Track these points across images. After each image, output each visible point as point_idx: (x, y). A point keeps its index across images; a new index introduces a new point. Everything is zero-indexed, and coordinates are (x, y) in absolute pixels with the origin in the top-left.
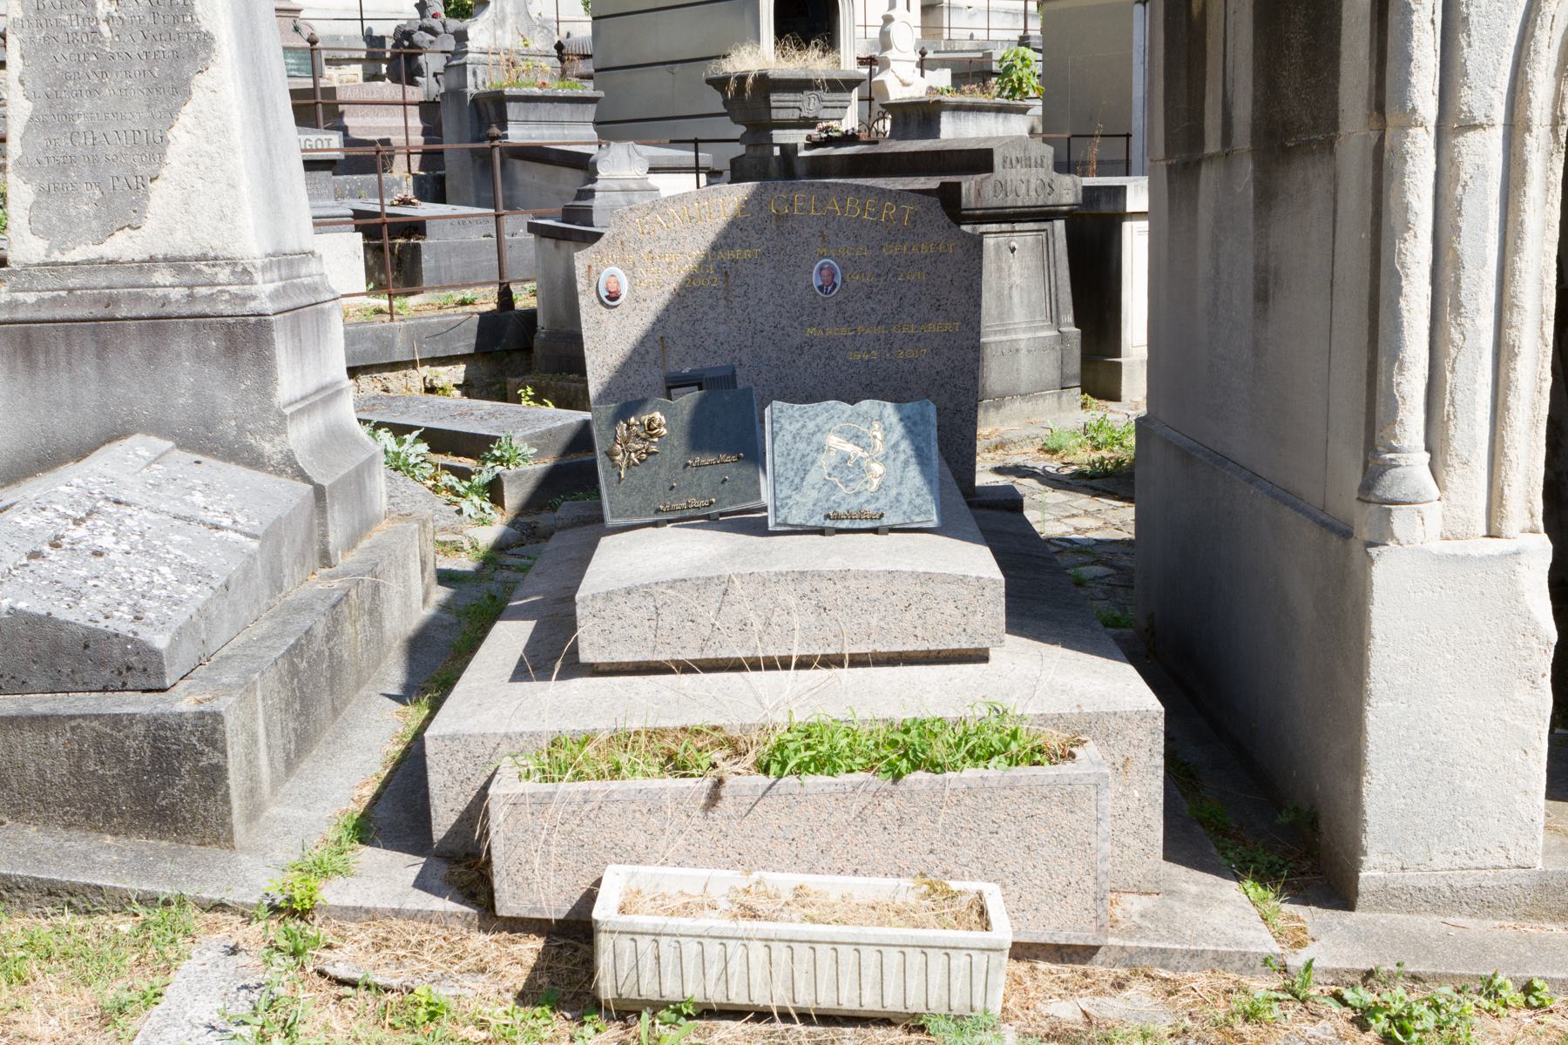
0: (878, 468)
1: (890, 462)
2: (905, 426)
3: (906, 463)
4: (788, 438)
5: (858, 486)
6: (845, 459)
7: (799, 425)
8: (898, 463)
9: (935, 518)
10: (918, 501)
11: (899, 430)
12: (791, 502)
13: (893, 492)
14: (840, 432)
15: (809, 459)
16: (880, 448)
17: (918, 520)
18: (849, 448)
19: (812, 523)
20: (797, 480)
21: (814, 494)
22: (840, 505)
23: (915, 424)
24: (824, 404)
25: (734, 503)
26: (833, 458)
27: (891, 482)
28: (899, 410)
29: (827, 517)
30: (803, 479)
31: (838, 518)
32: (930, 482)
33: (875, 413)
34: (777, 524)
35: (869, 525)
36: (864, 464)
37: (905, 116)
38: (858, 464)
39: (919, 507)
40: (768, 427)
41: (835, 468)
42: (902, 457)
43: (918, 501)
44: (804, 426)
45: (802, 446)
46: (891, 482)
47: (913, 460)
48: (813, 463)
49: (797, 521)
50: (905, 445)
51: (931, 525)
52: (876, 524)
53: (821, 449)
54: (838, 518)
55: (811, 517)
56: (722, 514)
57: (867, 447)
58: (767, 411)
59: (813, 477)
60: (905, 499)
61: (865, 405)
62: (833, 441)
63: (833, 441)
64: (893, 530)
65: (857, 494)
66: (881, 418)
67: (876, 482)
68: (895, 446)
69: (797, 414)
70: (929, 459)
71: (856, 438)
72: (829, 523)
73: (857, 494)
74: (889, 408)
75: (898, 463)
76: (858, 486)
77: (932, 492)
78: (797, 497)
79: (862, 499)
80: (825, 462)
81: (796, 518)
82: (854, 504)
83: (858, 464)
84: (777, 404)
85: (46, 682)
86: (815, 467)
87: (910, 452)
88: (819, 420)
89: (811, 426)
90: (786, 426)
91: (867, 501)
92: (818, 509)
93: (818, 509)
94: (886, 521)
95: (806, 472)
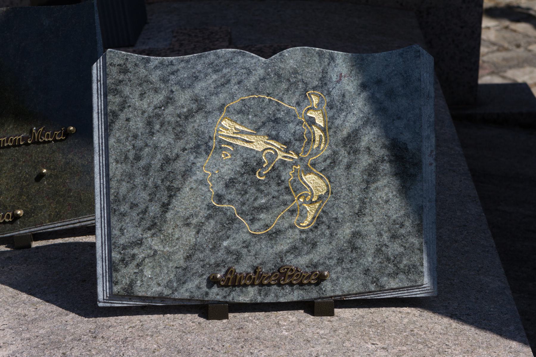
0: (314, 182)
1: (339, 171)
2: (372, 99)
3: (372, 173)
4: (138, 124)
5: (275, 219)
6: (251, 165)
7: (159, 98)
8: (357, 173)
9: (426, 280)
10: (395, 248)
11: (359, 107)
12: (140, 253)
13: (346, 231)
14: (242, 112)
15: (179, 165)
16: (320, 146)
17: (393, 285)
18: (259, 144)
19: (183, 293)
20: (154, 209)
21: (189, 236)
22: (238, 257)
23: (391, 94)
24: (211, 56)
25: (58, 217)
26: (226, 165)
27: (342, 211)
28: (359, 66)
29: (212, 282)
30: (165, 207)
31: (234, 281)
32: (419, 211)
33: (311, 74)
34: (113, 296)
35: (296, 295)
36: (288, 175)
37: (92, 247)
38: (276, 174)
39: (395, 260)
40: (97, 102)
41: (230, 184)
42: (365, 161)
43: (395, 248)
44: (169, 100)
45: (164, 140)
46: (342, 211)
47: (386, 167)
48: (186, 174)
49: (155, 290)
50: (370, 137)
51: (417, 293)
52: (312, 294)
53: (204, 145)
54: (234, 281)
55: (182, 282)
56: (37, 237)
57: (296, 142)
58: (96, 70)
59: (189, 201)
60: (369, 245)
61: (292, 57)
62: (227, 127)
63: (227, 127)
64: (344, 302)
65: (274, 235)
66: (323, 84)
67: (311, 211)
68: (351, 140)
69: (154, 77)
70: (418, 164)
71: (272, 124)
72: (216, 294)
73: (274, 235)
74: (341, 63)
75: (357, 173)
76: (275, 219)
77: (420, 229)
78: (155, 243)
79: (283, 246)
80: (211, 172)
81: (152, 282)
82: (267, 254)
83: (276, 174)
84: (116, 56)
85: (227, 44)
86: (191, 182)
87: (380, 152)
88: (199, 87)
89: (183, 98)
90: (135, 100)
91: (294, 250)
92: (196, 266)
93: (196, 266)
94: (329, 289)
95: (173, 192)
